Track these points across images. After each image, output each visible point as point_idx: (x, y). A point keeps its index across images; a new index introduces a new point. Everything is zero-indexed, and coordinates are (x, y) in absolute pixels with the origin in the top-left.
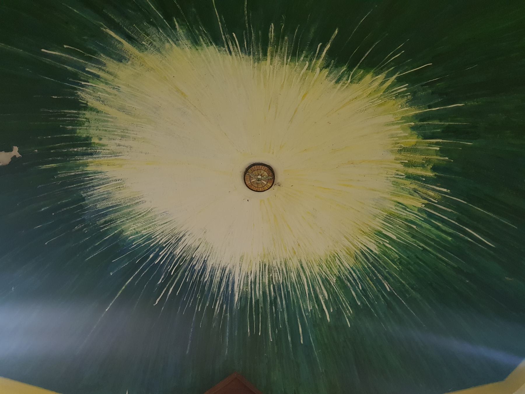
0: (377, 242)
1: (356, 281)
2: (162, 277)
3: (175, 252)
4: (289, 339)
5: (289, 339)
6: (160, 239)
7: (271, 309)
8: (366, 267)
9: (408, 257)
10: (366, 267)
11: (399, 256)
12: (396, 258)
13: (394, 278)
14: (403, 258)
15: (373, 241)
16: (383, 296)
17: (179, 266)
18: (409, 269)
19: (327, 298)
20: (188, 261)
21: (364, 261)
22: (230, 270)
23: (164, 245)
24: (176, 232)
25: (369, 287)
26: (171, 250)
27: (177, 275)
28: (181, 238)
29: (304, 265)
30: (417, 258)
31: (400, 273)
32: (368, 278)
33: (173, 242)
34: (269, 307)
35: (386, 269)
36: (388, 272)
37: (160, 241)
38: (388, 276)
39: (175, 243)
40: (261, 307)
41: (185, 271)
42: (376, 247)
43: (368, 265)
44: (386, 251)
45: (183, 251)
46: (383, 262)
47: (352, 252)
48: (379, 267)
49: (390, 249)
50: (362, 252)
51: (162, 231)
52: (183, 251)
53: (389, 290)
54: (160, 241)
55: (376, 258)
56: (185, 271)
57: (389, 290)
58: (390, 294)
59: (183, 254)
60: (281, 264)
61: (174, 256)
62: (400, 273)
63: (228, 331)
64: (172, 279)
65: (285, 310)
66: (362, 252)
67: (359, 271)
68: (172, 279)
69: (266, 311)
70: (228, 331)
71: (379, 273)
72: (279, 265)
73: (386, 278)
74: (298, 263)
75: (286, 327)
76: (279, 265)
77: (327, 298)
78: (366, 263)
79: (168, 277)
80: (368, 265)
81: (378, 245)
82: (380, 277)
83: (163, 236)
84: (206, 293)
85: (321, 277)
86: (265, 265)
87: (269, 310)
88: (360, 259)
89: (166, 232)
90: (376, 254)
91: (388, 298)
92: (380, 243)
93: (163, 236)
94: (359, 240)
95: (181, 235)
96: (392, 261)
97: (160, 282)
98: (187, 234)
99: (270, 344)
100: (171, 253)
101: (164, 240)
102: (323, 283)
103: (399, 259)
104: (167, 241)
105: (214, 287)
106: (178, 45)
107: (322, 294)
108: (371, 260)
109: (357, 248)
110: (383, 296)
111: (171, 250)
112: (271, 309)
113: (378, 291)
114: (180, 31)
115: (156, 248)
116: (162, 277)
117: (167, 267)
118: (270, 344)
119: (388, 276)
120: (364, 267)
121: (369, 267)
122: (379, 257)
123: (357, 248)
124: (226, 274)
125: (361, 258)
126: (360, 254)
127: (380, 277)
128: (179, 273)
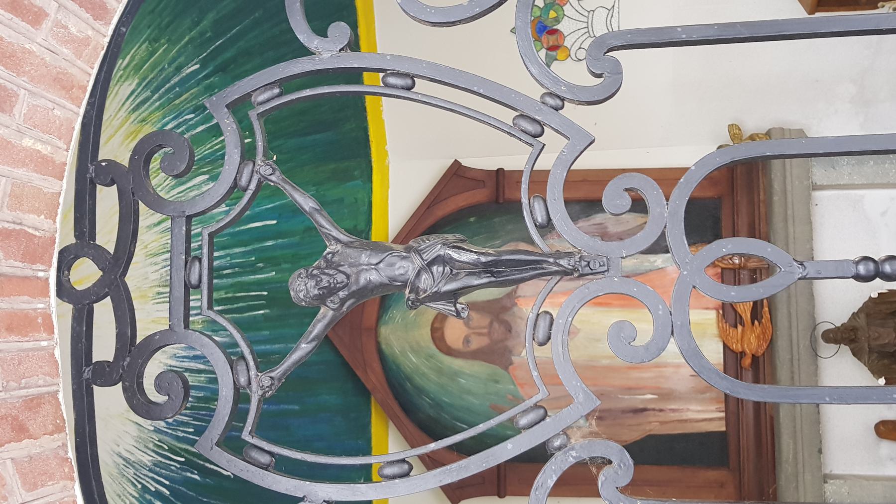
0: (118, 81)
1: (180, 123)
2: (189, 474)
3: (149, 464)
4: (270, 243)
5: (270, 243)
6: (131, 498)
7: (227, 276)
8: (158, 103)
9: (149, 27)
10: (158, 103)
11: (144, 42)
12: (147, 47)
13: (179, 54)
14: (150, 34)
15: (117, 88)
16: (207, 77)
17: (171, 450)
18: (168, 26)
19: (207, 177)
20: (161, 437)
21: (150, 106)
22: (171, 357)
23: (140, 486)
24: (116, 471)
25: (191, 101)
26: (145, 472)
27: (186, 451)
28: (124, 459)
29: (156, 221)
30: (153, 11)
31: (172, 43)
32: (177, 102)
33: (132, 471)
34: (225, 280)
35: (163, 69)
36: (170, 65)
37: (134, 497)
38: (174, 65)
39: (133, 467)
40: (226, 293)
41: (178, 438)
42: (127, 83)
43: (156, 101)
44: (136, 65)
45: (145, 450)
46: (152, 72)
47: (133, 129)
48: (160, 79)
49: (133, 58)
50: (135, 110)
51: (117, 498)
52: (145, 450)
53: (198, 66)
54: (134, 497)
55: (144, 84)
56: (178, 438)
57: (198, 66)
58: (204, 64)
59: (149, 449)
60: (156, 264)
61: (155, 465)
62: (172, 43)
63: (263, 347)
64: (192, 458)
65: (228, 251)
66: (135, 110)
67: (164, 118)
68: (192, 458)
69: (232, 285)
70: (263, 347)
71: (169, 81)
72: (157, 267)
73: (179, 69)
74: (152, 231)
75: (254, 250)
76: (157, 267)
77: (207, 177)
78: (153, 103)
79: (189, 465)
80: (156, 101)
81: (123, 79)
82: (176, 79)
83: (126, 493)
84: (209, 394)
85: (173, 188)
86: (159, 293)
87: (230, 281)
88: (144, 115)
89: (119, 490)
90: (139, 85)
91: (211, 69)
92: (121, 77)
93: (126, 493)
94: (113, 115)
95: (121, 461)
96: (152, 54)
97: (197, 477)
98: (117, 449)
99: (280, 276)
100: (150, 470)
101: (131, 490)
102: (183, 184)
103: (150, 43)
104: (133, 483)
105: (199, 382)
106: (587, 417)
107: (199, 185)
108: (148, 93)
109: (127, 119)
110: (207, 77)
111: (145, 472)
112: (227, 276)
113: (198, 85)
114: (709, 193)
115: (145, 499)
116: (189, 474)
117: (172, 471)
118: (280, 276)
119: (174, 65)
120: (158, 109)
121: (159, 99)
122: (144, 79)
123: (127, 119)
124: (178, 364)
125: (143, 112)
126: (137, 113)
127: (176, 79)
128: (180, 448)
